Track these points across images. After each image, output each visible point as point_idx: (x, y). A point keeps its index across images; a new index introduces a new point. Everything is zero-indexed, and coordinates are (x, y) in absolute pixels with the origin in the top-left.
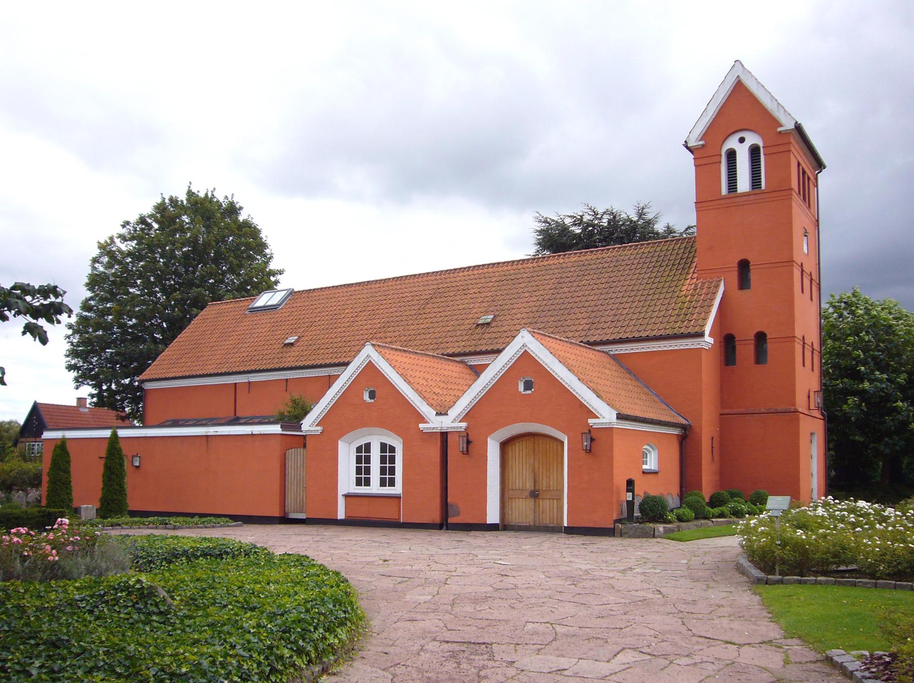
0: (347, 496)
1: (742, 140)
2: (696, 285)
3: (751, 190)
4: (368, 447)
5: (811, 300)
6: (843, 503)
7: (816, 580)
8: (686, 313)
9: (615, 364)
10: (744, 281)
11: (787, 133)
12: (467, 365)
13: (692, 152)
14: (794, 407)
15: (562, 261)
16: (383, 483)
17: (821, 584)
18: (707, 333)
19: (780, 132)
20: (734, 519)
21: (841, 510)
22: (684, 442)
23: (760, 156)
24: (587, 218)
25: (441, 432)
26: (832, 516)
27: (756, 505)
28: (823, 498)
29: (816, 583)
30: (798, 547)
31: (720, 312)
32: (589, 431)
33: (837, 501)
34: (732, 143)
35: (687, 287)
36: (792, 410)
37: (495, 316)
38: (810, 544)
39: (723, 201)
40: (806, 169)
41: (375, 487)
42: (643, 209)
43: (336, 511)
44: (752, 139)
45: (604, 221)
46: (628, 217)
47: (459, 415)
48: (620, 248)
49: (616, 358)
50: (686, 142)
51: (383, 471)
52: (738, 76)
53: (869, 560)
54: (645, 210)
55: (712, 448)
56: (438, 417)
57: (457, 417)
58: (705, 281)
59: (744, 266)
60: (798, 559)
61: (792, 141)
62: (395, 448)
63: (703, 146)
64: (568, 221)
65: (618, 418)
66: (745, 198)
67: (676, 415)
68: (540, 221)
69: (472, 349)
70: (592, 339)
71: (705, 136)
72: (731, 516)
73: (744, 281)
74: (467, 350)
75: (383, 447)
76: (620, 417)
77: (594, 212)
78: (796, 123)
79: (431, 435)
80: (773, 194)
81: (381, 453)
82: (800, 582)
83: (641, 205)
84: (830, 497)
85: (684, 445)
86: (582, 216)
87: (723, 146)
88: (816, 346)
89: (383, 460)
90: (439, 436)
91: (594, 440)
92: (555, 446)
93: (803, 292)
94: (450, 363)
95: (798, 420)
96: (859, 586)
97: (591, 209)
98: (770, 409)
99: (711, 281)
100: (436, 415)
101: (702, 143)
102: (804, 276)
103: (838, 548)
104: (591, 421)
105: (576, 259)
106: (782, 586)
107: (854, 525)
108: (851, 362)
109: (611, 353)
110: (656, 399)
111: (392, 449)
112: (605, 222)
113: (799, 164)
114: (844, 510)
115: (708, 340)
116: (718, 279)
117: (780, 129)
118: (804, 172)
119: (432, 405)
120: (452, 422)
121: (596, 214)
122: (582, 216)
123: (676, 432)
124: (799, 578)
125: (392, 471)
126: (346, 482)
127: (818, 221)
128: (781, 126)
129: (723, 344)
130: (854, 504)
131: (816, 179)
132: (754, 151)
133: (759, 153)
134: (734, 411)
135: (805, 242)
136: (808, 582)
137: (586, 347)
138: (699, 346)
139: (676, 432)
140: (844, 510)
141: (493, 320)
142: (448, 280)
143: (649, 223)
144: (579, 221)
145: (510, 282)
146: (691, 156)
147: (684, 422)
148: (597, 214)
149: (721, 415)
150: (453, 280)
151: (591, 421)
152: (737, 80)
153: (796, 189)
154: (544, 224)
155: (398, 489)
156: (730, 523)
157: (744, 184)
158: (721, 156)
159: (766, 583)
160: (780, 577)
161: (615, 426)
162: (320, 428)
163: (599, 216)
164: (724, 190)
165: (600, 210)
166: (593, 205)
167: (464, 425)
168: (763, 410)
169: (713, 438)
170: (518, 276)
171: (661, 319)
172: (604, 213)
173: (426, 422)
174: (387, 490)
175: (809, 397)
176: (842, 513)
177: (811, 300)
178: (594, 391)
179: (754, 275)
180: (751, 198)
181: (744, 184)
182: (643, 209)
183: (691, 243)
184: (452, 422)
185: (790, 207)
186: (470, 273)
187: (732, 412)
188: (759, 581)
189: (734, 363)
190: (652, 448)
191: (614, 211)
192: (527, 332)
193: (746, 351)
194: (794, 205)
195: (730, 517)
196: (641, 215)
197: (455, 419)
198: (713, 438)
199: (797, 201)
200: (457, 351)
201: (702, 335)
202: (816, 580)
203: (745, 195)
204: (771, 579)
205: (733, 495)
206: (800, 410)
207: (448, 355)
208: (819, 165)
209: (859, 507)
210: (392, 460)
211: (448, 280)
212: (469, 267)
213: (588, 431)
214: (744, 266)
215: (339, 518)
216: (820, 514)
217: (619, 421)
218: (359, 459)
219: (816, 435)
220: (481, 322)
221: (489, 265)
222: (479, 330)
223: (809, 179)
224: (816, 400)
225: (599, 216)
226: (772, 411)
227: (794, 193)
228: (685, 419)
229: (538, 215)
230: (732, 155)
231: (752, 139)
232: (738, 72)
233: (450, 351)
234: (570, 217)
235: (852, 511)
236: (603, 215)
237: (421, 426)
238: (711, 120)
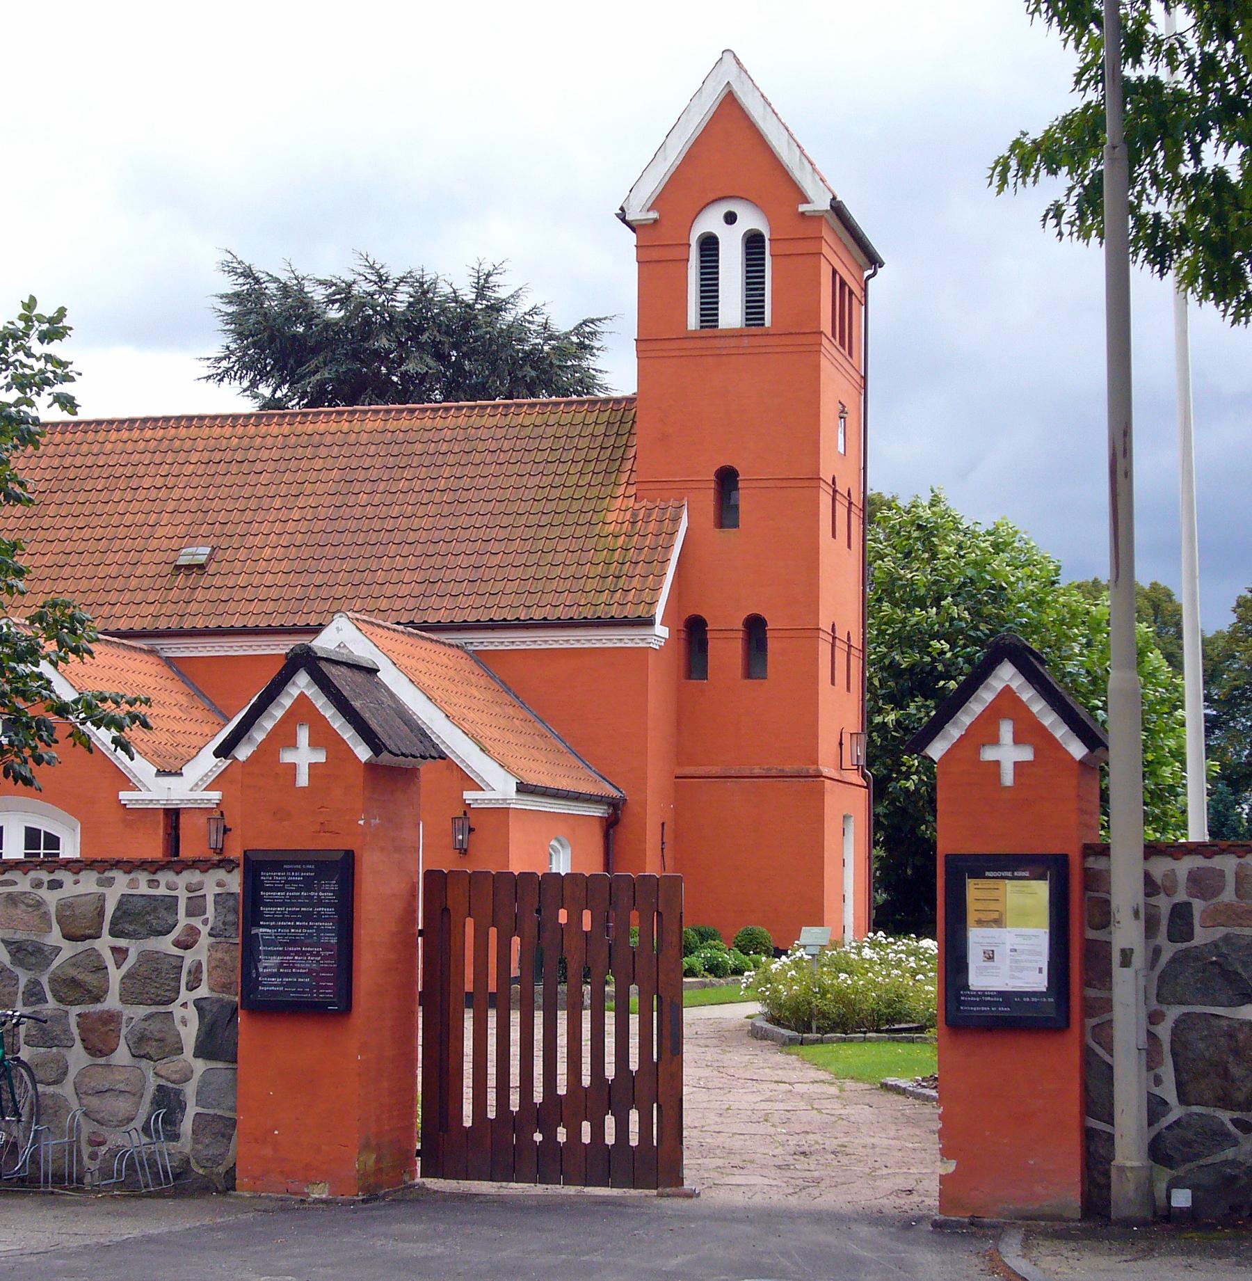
1: (730, 218)
2: (634, 515)
3: (744, 326)
5: (849, 546)
6: (900, 943)
7: (865, 1038)
8: (617, 573)
9: (482, 672)
10: (726, 513)
11: (816, 218)
12: (160, 657)
13: (634, 230)
14: (814, 767)
15: (345, 426)
17: (870, 1041)
18: (658, 619)
19: (803, 213)
20: (710, 978)
21: (896, 952)
22: (611, 831)
24: (362, 287)
25: (164, 809)
26: (883, 961)
27: (748, 954)
28: (871, 934)
29: (865, 1039)
30: (841, 997)
31: (679, 574)
32: (465, 813)
33: (891, 940)
34: (710, 221)
35: (616, 514)
36: (812, 772)
37: (214, 549)
38: (856, 993)
39: (691, 344)
40: (842, 271)
42: (489, 275)
44: (750, 220)
45: (400, 297)
46: (455, 292)
47: (206, 775)
48: (472, 408)
49: (480, 658)
50: (622, 209)
52: (728, 82)
53: (931, 1010)
54: (491, 279)
55: (663, 843)
56: (159, 779)
57: (201, 780)
58: (650, 505)
59: (727, 479)
60: (841, 1012)
61: (825, 233)
62: (58, 839)
63: (656, 221)
64: (318, 294)
65: (518, 791)
66: (734, 342)
67: (599, 779)
68: (233, 271)
69: (174, 624)
70: (432, 618)
71: (658, 203)
72: (706, 973)
73: (726, 513)
74: (162, 624)
76: (523, 788)
77: (380, 276)
78: (834, 198)
79: (144, 813)
80: (785, 340)
81: (26, 849)
82: (844, 1040)
83: (487, 268)
84: (881, 933)
85: (611, 837)
86: (350, 286)
87: (692, 233)
88: (856, 642)
90: (162, 816)
93: (834, 536)
94: (125, 653)
95: (820, 795)
96: (917, 1042)
97: (372, 267)
98: (769, 769)
99: (663, 505)
101: (654, 215)
102: (837, 502)
103: (892, 995)
104: (468, 795)
105: (379, 425)
106: (821, 1046)
107: (914, 973)
108: (922, 658)
109: (471, 648)
110: (561, 746)
112: (403, 298)
113: (834, 272)
114: (902, 952)
115: (661, 631)
116: (676, 504)
117: (803, 208)
118: (843, 284)
119: (146, 754)
120: (191, 790)
121: (382, 279)
122: (350, 286)
123: (598, 811)
124: (844, 1035)
127: (865, 378)
128: (806, 200)
129: (683, 635)
130: (915, 944)
131: (865, 290)
132: (753, 242)
134: (700, 771)
135: (841, 430)
136: (855, 1040)
137: (423, 638)
138: (642, 645)
139: (598, 811)
140: (902, 952)
141: (211, 557)
142: (85, 448)
143: (496, 308)
144: (343, 294)
145: (234, 468)
146: (632, 237)
147: (615, 793)
148: (387, 280)
149: (676, 777)
150: (96, 448)
151: (468, 795)
152: (726, 91)
153: (828, 332)
154: (241, 280)
156: (704, 985)
157: (731, 313)
158: (689, 245)
159: (801, 1044)
160: (820, 1035)
161: (512, 806)
163: (390, 286)
164: (693, 321)
165: (395, 273)
166: (379, 258)
167: (216, 795)
168: (757, 771)
169: (663, 824)
170: (251, 455)
171: (568, 582)
172: (402, 280)
173: (135, 788)
175: (841, 744)
176: (898, 956)
177: (849, 546)
178: (474, 738)
179: (745, 498)
180: (746, 342)
181: (731, 313)
182: (489, 275)
183: (620, 413)
184: (191, 790)
185: (817, 368)
186: (136, 434)
187: (700, 773)
188: (792, 1041)
189: (704, 675)
190: (562, 845)
191: (427, 278)
192: (347, 620)
194: (824, 363)
195: (703, 976)
196: (481, 289)
197: (197, 784)
198: (663, 824)
199: (829, 348)
200: (138, 625)
201: (649, 622)
202: (865, 1038)
204: (807, 1037)
205: (703, 937)
206: (826, 771)
207: (119, 634)
208: (874, 261)
209: (922, 947)
211: (85, 448)
212: (132, 421)
213: (461, 815)
214: (727, 479)
216: (868, 957)
217: (519, 797)
219: (853, 819)
220: (183, 561)
221: (179, 419)
222: (180, 580)
223: (851, 293)
224: (855, 751)
225: (390, 286)
226: (774, 773)
227: (825, 341)
228: (614, 787)
229: (229, 257)
230: (709, 245)
231: (750, 220)
232: (729, 73)
233: (123, 625)
234: (321, 283)
235: (914, 953)
236: (397, 284)
237: (124, 796)
238: (673, 169)
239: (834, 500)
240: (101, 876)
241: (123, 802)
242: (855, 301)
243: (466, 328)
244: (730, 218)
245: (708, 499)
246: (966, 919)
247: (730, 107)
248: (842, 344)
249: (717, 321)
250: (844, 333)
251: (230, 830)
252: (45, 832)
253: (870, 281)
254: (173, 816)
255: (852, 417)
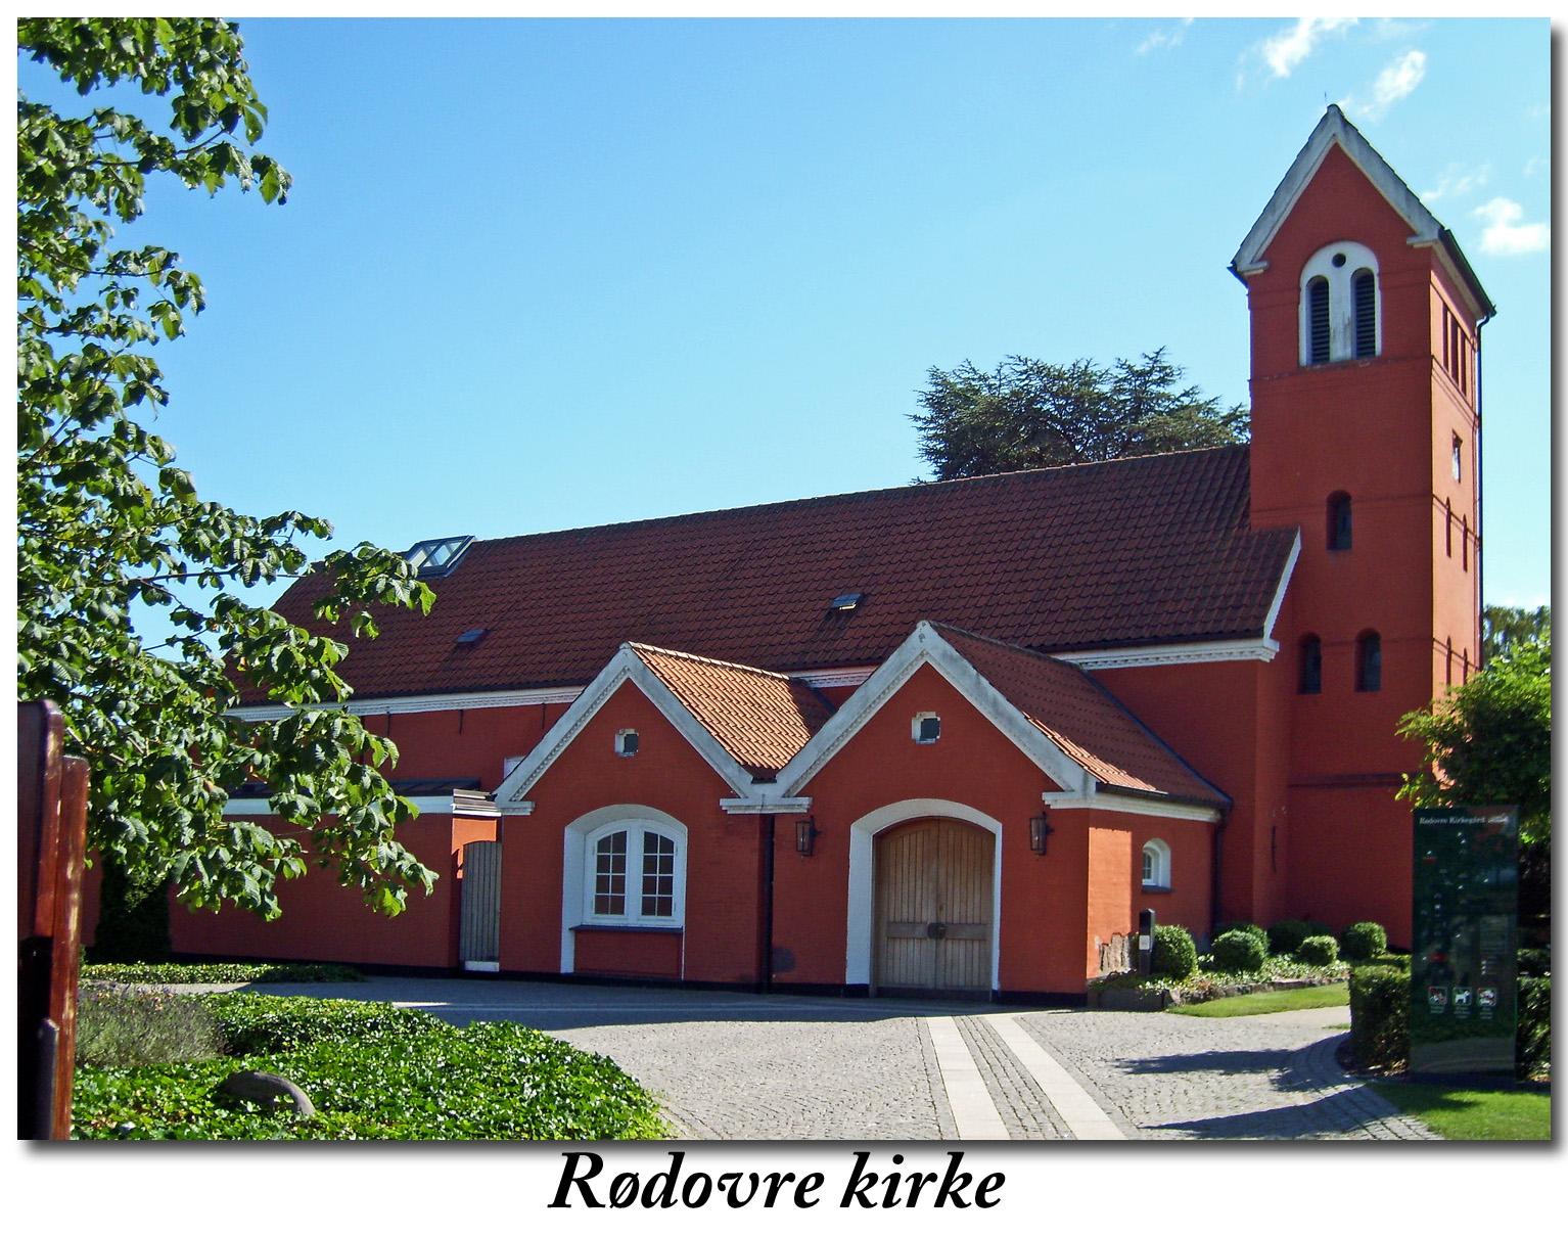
0: (580, 931)
1: (1339, 260)
4: (620, 840)
5: (1465, 568)
16: (648, 908)
18: (1269, 625)
23: (1373, 291)
34: (1319, 265)
41: (633, 915)
43: (990, 982)
50: (1233, 262)
51: (648, 885)
59: (1339, 504)
67: (1207, 785)
75: (650, 840)
89: (649, 864)
90: (757, 822)
91: (1052, 831)
92: (972, 838)
100: (752, 782)
101: (1265, 264)
102: (1452, 525)
111: (668, 845)
113: (1446, 309)
115: (1266, 649)
118: (1455, 324)
125: (667, 885)
126: (579, 907)
127: (1479, 417)
132: (1362, 283)
133: (1373, 286)
153: (1441, 358)
155: (677, 919)
157: (1341, 348)
162: (805, 801)
164: (1304, 355)
169: (1274, 830)
173: (735, 796)
174: (654, 921)
177: (1465, 568)
181: (1341, 348)
193: (1340, 666)
203: (1343, 364)
208: (1488, 310)
210: (668, 865)
214: (1339, 504)
215: (563, 971)
218: (602, 864)
223: (1464, 336)
230: (1320, 288)
231: (1361, 257)
237: (724, 803)
239: (1449, 521)
240: (1153, 918)
241: (724, 809)
242: (1468, 346)
243: (1137, 413)
244: (1339, 260)
245: (1320, 522)
246: (827, 720)
247: (1336, 155)
248: (1455, 375)
249: (1328, 353)
250: (1457, 373)
251: (1052, 831)
252: (661, 837)
253: (1483, 328)
254: (767, 822)
255: (1466, 448)
